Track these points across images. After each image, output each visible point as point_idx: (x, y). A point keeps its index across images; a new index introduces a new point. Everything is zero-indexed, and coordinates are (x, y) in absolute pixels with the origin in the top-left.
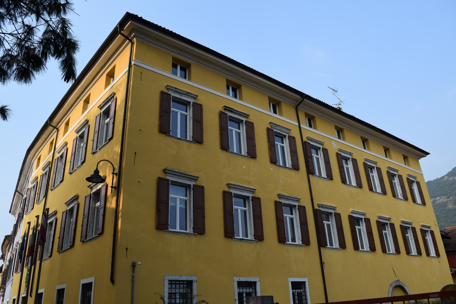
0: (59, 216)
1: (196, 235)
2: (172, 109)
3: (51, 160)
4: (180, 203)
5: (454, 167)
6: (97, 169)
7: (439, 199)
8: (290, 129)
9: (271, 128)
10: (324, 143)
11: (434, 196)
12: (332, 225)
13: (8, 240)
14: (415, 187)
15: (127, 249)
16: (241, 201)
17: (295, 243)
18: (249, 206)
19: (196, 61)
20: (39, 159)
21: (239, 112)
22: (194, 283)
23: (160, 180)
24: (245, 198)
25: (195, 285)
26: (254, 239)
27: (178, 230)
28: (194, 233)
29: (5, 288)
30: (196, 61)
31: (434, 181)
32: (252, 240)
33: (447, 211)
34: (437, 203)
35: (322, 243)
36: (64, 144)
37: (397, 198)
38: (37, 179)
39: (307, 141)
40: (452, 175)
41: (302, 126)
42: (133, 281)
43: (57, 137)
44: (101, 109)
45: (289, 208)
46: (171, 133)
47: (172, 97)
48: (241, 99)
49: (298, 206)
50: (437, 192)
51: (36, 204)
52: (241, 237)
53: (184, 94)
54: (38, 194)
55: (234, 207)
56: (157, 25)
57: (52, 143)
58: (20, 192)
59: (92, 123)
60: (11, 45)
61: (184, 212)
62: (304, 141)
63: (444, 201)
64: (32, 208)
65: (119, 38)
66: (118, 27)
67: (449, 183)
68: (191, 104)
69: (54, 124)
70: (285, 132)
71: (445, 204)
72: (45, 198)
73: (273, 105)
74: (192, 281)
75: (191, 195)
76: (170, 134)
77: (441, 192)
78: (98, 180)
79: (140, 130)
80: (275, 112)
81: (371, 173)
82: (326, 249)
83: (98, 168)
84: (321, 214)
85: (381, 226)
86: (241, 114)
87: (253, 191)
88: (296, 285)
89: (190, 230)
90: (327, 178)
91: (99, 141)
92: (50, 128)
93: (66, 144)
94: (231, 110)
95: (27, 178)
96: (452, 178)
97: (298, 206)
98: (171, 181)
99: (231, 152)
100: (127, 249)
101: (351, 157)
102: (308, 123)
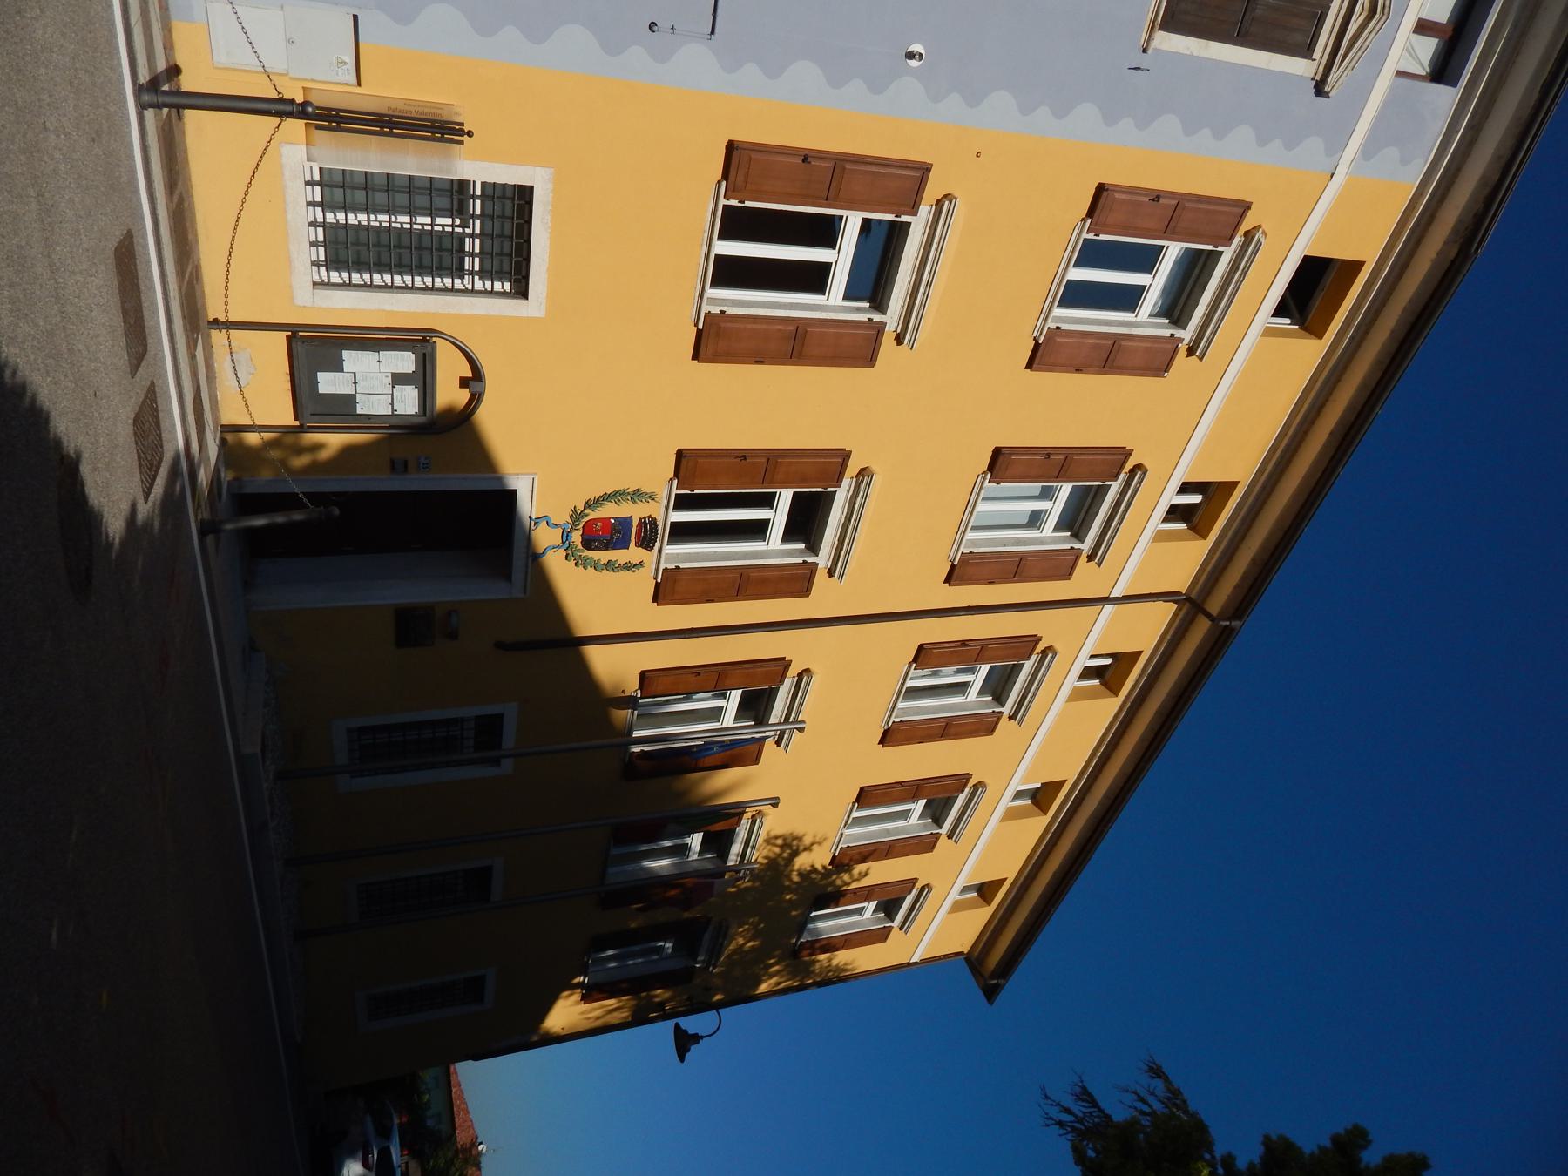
26: (705, 309)
37: (970, 505)
41: (1108, 609)
80: (1087, 673)
88: (490, 729)
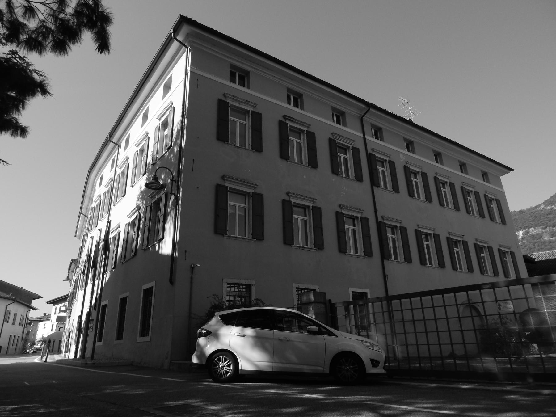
0: (122, 230)
1: (255, 241)
2: (231, 118)
3: (113, 177)
4: (239, 210)
5: (553, 195)
6: (155, 176)
7: (533, 230)
8: (353, 140)
9: (333, 138)
10: (391, 155)
11: (527, 227)
12: (397, 239)
13: (74, 264)
14: (494, 206)
15: (186, 251)
16: (302, 210)
17: (357, 254)
18: (309, 216)
19: (254, 68)
20: (102, 178)
21: (300, 121)
22: (252, 287)
23: (218, 186)
24: (305, 208)
25: (253, 289)
27: (237, 235)
28: (253, 239)
29: (71, 309)
30: (254, 68)
31: (529, 210)
32: (312, 248)
33: (542, 243)
34: (530, 234)
35: (385, 255)
36: (125, 158)
38: (100, 197)
39: (371, 152)
40: (550, 204)
41: (367, 137)
42: (191, 282)
43: (118, 154)
44: (159, 120)
45: (351, 220)
46: (229, 141)
47: (230, 105)
48: (302, 108)
49: (361, 217)
50: (531, 223)
51: (100, 221)
52: (301, 245)
53: (243, 102)
54: (101, 211)
55: (294, 216)
56: (220, 32)
57: (113, 161)
58: (85, 214)
59: (152, 136)
60: (45, 15)
61: (243, 218)
62: (369, 153)
63: (538, 232)
64: (96, 226)
65: (175, 45)
66: (172, 32)
67: (545, 212)
68: (250, 112)
69: (115, 140)
70: (348, 144)
71: (540, 236)
72: (108, 214)
73: (337, 116)
74: (251, 284)
75: (250, 202)
76: (228, 142)
77: (535, 222)
78: (157, 186)
79: (198, 137)
81: (443, 188)
82: (390, 262)
83: (156, 175)
84: (386, 228)
85: (452, 243)
86: (301, 123)
87: (314, 200)
89: (249, 236)
90: (392, 191)
91: (159, 152)
92: (111, 145)
93: (128, 159)
94: (292, 120)
95: (91, 200)
96: (550, 207)
97: (361, 217)
98: (230, 188)
99: (292, 162)
100: (186, 251)
101: (421, 171)
102: (374, 134)
